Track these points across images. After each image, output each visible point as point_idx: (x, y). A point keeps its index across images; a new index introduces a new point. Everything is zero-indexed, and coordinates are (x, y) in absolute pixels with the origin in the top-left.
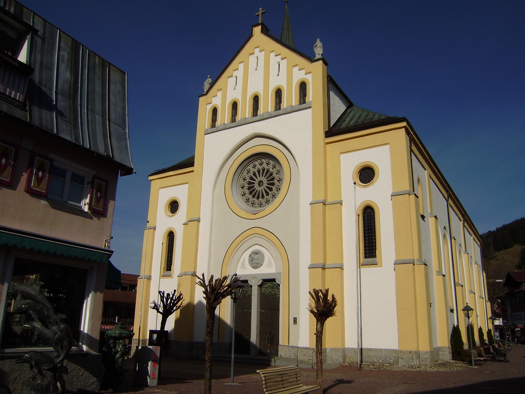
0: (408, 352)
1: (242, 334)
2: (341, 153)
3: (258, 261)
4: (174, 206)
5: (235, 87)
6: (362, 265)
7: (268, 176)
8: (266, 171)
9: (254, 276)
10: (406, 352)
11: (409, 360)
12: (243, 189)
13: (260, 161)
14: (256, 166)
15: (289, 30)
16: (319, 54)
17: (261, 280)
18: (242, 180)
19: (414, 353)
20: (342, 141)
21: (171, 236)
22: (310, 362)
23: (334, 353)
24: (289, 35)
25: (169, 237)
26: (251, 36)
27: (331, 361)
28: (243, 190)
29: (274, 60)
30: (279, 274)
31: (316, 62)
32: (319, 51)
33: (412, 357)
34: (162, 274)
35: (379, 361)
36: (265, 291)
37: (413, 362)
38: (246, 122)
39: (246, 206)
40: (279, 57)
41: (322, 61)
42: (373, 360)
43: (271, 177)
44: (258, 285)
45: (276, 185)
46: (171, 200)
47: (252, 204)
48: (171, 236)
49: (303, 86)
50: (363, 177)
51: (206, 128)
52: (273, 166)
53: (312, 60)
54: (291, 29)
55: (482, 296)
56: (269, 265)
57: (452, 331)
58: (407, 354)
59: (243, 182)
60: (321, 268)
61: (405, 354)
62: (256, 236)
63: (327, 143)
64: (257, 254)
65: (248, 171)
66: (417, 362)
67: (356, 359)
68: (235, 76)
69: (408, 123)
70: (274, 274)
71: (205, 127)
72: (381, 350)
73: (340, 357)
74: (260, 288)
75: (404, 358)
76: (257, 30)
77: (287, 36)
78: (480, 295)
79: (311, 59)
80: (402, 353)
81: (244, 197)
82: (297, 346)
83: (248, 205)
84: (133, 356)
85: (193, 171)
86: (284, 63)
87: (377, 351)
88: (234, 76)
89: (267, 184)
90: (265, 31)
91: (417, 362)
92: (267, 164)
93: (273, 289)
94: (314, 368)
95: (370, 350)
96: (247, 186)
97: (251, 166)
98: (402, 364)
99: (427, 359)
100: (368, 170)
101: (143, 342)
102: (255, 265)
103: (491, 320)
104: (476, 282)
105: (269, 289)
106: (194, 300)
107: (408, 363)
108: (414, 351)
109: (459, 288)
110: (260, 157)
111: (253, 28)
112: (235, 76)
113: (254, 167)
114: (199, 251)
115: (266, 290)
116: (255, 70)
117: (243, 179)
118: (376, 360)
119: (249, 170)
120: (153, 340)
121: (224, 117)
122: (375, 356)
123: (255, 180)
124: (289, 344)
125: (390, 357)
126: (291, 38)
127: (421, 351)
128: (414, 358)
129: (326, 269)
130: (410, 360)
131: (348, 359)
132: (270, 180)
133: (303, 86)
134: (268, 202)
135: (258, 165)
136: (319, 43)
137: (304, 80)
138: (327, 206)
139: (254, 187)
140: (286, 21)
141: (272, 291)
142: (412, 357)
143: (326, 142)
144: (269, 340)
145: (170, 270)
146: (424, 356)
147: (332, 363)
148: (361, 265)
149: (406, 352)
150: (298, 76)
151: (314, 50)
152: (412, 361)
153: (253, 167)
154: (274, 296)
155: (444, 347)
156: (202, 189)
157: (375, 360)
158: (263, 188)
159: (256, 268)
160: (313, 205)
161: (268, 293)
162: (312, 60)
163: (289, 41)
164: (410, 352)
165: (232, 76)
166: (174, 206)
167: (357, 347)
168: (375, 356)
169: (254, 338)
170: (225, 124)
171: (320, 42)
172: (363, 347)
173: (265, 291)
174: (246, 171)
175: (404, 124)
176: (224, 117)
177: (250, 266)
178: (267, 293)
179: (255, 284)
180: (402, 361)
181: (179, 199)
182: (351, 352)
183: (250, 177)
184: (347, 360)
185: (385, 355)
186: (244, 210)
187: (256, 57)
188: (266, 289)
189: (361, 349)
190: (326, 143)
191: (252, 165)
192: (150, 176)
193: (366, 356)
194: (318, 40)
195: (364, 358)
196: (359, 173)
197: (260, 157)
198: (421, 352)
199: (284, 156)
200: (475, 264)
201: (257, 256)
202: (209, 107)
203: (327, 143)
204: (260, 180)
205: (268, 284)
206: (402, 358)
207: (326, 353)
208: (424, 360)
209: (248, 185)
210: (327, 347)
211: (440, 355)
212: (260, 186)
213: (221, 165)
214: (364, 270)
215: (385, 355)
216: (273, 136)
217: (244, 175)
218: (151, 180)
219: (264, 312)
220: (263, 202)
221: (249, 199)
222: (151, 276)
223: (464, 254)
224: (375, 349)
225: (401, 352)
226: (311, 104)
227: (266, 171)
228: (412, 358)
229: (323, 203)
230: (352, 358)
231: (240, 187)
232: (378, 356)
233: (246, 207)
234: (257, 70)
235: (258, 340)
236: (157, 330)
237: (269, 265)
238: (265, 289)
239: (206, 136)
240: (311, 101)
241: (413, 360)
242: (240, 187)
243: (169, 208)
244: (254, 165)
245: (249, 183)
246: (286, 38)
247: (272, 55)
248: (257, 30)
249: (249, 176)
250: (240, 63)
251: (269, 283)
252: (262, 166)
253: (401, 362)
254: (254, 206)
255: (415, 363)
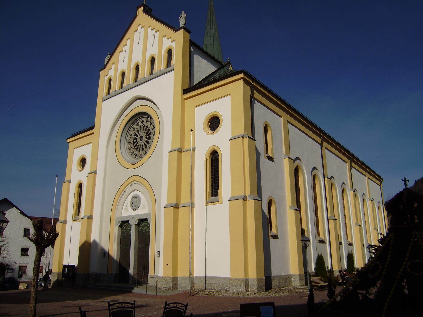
0: (237, 279)
1: (126, 266)
2: (196, 106)
3: (137, 204)
4: (83, 162)
5: (124, 59)
6: (207, 203)
7: (148, 131)
8: (145, 127)
9: (133, 217)
10: (236, 280)
11: (238, 287)
12: (130, 144)
13: (141, 120)
14: (139, 124)
15: (213, 14)
16: (183, 24)
17: (137, 220)
18: (129, 136)
19: (242, 281)
20: (194, 97)
21: (80, 186)
22: (163, 289)
23: (183, 282)
24: (213, 18)
25: (80, 188)
26: (136, 16)
27: (181, 288)
28: (129, 145)
29: (151, 33)
30: (149, 214)
31: (179, 31)
32: (182, 22)
33: (240, 284)
34: (73, 219)
35: (218, 288)
36: (142, 229)
37: (241, 288)
38: (129, 88)
39: (130, 158)
40: (154, 30)
41: (183, 29)
42: (214, 287)
43: (149, 133)
44: (136, 225)
45: (152, 139)
46: (81, 158)
47: (135, 156)
48: (80, 186)
49: (170, 52)
50: (213, 125)
51: (104, 96)
52: (150, 123)
53: (176, 29)
54: (214, 13)
55: (377, 228)
56: (144, 207)
57: (316, 260)
58: (236, 282)
59: (130, 139)
60: (173, 207)
61: (235, 282)
62: (134, 183)
63: (186, 99)
64: (136, 198)
65: (133, 128)
66: (244, 289)
67: (201, 286)
68: (124, 51)
69: (245, 73)
70: (146, 214)
71: (103, 95)
72: (220, 278)
73: (187, 285)
74: (139, 226)
75: (234, 285)
76: (140, 10)
77: (212, 19)
78: (374, 227)
79: (175, 28)
80: (233, 280)
81: (130, 151)
82: (158, 275)
83: (133, 157)
84: (52, 286)
85: (93, 133)
86: (157, 34)
87: (217, 279)
88: (123, 51)
89: (146, 139)
90: (148, 11)
91: (244, 289)
92: (146, 121)
93: (147, 227)
94: (158, 294)
95: (212, 278)
96: (132, 141)
97: (135, 125)
98: (233, 291)
99: (254, 285)
100: (216, 120)
101: (59, 275)
102: (134, 207)
103: (368, 248)
104: (370, 216)
105: (145, 227)
106: (91, 239)
107: (237, 289)
108: (242, 279)
109: (331, 222)
110: (143, 115)
111: (138, 9)
112: (124, 51)
113: (138, 124)
114: (95, 198)
115: (142, 228)
116: (152, 46)
117: (130, 136)
118: (216, 287)
119: (134, 128)
120: (65, 273)
121: (116, 86)
122: (215, 283)
123: (138, 136)
124: (154, 274)
125: (227, 284)
126: (214, 21)
127: (250, 278)
128: (242, 285)
129: (179, 208)
130: (239, 287)
131: (196, 287)
132: (148, 134)
133: (170, 52)
134: (141, 156)
135: (140, 123)
136: (183, 15)
137: (169, 47)
138: (183, 153)
139: (137, 141)
140: (210, 7)
141: (147, 228)
142: (240, 284)
143: (184, 98)
144: (144, 271)
145: (217, 195)
146: (252, 283)
147: (182, 290)
148: (208, 203)
149: (236, 280)
150: (167, 44)
151: (179, 21)
152: (240, 288)
153: (137, 125)
154: (147, 234)
155: (295, 274)
156: (99, 146)
157: (216, 287)
158: (143, 142)
159: (135, 210)
160: (171, 152)
161: (144, 230)
162: (176, 29)
163: (213, 23)
164: (239, 280)
165: (122, 51)
166: (83, 162)
167: (189, 276)
168: (216, 284)
169: (131, 270)
170: (115, 91)
171: (185, 13)
172: (207, 276)
173: (142, 229)
174: (132, 129)
175: (242, 75)
176: (116, 86)
177: (131, 208)
178: (143, 231)
179: (133, 223)
180: (233, 288)
181: (85, 155)
182: (198, 280)
183: (134, 134)
184: (196, 287)
185: (223, 283)
186: (127, 162)
187: (153, 35)
188: (142, 228)
189: (206, 277)
190: (184, 99)
191: (136, 123)
192: (68, 139)
193: (209, 283)
194: (183, 12)
195: (207, 286)
196: (209, 122)
197: (143, 115)
198: (250, 279)
199: (156, 113)
200: (369, 200)
201: (136, 199)
202: (107, 78)
203: (186, 99)
204: (141, 135)
205: (144, 223)
206: (232, 285)
207: (177, 281)
208: (252, 287)
209: (133, 140)
210: (178, 276)
211: (292, 282)
212: (141, 141)
213: (112, 125)
214: (210, 207)
215: (223, 283)
216: (148, 97)
217: (130, 133)
218: (69, 142)
219: (141, 247)
220: (142, 154)
221: (133, 152)
222: (67, 221)
223: (350, 192)
224: (216, 277)
225: (232, 280)
226: (174, 67)
227: (145, 127)
228: (240, 285)
229: (178, 151)
230: (199, 286)
231: (127, 143)
232: (217, 284)
233: (130, 159)
234: (153, 46)
235: (136, 271)
236: (69, 264)
237: (144, 207)
238: (142, 227)
239: (103, 102)
240: (174, 64)
241: (241, 286)
242: (127, 143)
243: (80, 164)
244: (138, 123)
245: (135, 139)
246: (211, 20)
247: (150, 29)
248: (140, 10)
249: (133, 133)
250: (128, 39)
251: (145, 222)
252: (143, 124)
253: (232, 289)
254: (136, 158)
255: (243, 290)
